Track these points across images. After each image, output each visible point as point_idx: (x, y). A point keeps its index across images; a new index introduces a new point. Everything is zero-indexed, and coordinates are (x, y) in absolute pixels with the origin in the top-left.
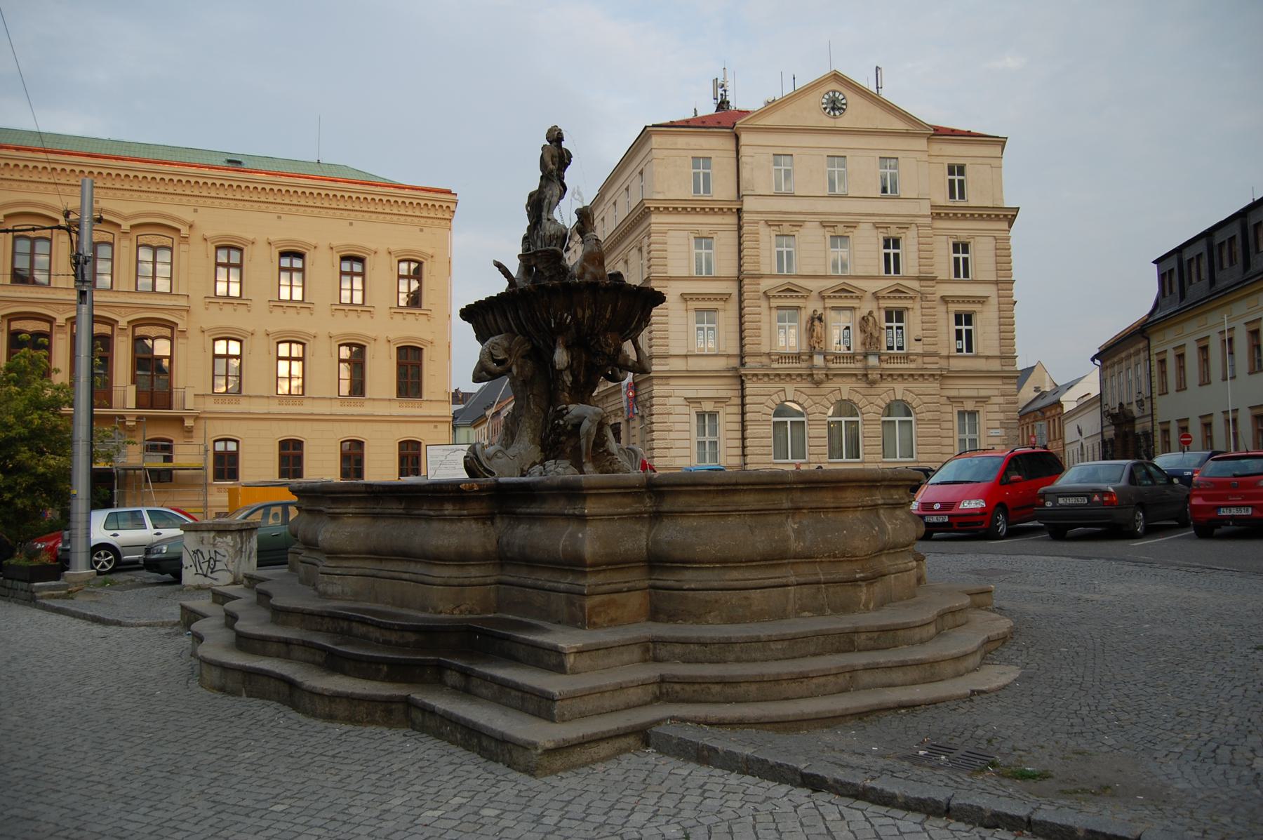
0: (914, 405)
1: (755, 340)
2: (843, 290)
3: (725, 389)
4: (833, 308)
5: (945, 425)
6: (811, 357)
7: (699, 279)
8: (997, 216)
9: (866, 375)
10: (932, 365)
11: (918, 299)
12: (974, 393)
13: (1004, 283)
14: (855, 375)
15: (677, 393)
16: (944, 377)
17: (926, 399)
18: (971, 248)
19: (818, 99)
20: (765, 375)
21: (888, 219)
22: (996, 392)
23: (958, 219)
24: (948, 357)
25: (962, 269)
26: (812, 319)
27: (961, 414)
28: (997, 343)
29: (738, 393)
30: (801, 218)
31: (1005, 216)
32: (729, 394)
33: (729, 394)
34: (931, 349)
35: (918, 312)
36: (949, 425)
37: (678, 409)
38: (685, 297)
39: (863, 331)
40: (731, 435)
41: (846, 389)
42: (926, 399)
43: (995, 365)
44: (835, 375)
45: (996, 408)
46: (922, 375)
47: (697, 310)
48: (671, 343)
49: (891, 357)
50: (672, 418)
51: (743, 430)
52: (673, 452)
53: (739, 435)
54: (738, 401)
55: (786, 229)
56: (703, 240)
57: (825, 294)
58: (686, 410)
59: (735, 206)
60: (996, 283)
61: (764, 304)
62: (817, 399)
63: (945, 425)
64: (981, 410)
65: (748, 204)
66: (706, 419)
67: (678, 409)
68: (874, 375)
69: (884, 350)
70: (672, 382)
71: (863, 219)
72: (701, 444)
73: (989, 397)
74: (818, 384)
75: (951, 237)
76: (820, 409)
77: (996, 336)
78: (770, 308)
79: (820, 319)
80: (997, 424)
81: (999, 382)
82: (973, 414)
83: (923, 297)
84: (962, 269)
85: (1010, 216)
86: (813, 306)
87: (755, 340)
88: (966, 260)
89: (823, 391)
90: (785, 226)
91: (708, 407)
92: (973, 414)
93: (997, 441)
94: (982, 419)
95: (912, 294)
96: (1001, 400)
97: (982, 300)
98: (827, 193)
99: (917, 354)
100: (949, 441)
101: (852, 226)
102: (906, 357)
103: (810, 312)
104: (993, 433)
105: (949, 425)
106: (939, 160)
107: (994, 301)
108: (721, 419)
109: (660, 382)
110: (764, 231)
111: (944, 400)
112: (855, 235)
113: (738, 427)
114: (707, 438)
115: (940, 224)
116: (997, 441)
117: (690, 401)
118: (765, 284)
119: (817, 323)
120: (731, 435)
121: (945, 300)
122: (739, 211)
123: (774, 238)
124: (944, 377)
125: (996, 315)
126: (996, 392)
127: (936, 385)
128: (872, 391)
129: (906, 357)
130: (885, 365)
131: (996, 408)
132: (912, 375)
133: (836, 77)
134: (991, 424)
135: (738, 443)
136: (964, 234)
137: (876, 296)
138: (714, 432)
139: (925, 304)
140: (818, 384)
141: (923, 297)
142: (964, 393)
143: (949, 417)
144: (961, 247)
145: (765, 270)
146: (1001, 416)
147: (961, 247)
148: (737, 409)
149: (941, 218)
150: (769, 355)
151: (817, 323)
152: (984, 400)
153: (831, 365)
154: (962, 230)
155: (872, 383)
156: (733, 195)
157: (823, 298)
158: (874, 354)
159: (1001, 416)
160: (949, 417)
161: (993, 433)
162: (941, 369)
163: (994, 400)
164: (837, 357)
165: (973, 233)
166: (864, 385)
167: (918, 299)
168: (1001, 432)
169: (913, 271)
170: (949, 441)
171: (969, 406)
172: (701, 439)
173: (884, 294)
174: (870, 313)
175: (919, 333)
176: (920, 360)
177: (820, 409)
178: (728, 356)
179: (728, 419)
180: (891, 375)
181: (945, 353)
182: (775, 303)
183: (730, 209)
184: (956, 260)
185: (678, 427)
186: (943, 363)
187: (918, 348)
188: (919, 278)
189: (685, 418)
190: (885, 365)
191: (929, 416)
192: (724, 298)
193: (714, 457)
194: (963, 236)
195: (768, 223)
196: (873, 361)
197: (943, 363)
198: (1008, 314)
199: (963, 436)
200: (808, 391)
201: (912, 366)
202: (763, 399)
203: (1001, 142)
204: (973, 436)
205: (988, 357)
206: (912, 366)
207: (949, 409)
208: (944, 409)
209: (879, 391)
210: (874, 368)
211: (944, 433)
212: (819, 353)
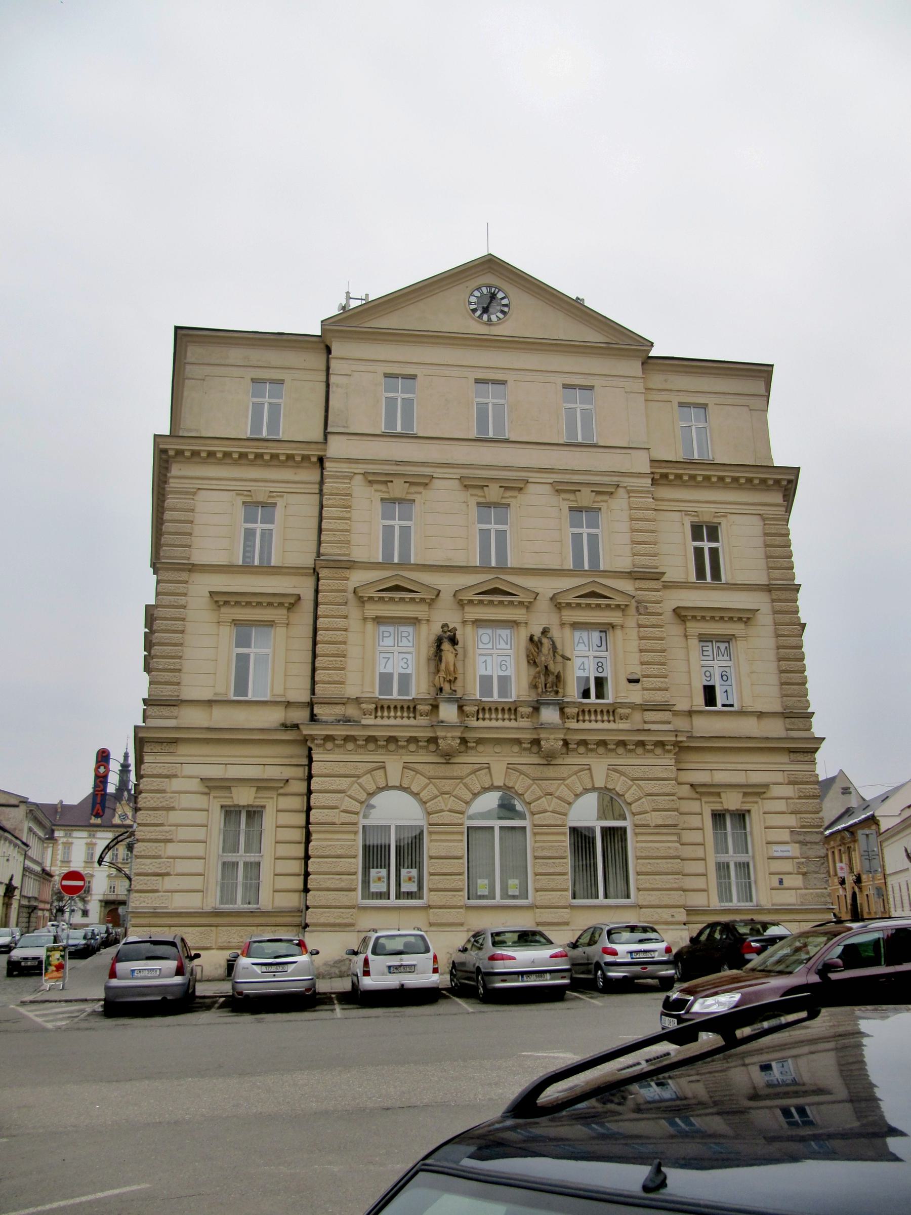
0: (629, 797)
1: (335, 675)
2: (397, 588)
3: (272, 763)
4: (478, 623)
5: (688, 837)
6: (435, 707)
7: (246, 568)
8: (721, 479)
9: (536, 742)
10: (660, 725)
11: (632, 610)
12: (739, 778)
13: (783, 590)
14: (518, 742)
15: (188, 770)
16: (682, 749)
17: (650, 787)
18: (722, 533)
19: (466, 296)
20: (347, 739)
21: (577, 478)
22: (779, 777)
23: (698, 486)
24: (690, 713)
25: (708, 567)
26: (439, 641)
27: (718, 817)
28: (774, 691)
29: (301, 772)
30: (427, 471)
31: (777, 482)
32: (288, 772)
33: (288, 772)
34: (659, 697)
35: (633, 633)
36: (696, 837)
37: (186, 801)
38: (220, 600)
39: (532, 662)
40: (283, 850)
41: (499, 765)
42: (650, 787)
43: (775, 728)
44: (480, 741)
45: (781, 806)
46: (642, 744)
47: (235, 623)
48: (186, 679)
49: (583, 712)
50: (174, 817)
51: (308, 840)
52: (169, 883)
53: (300, 851)
54: (302, 787)
55: (398, 489)
56: (259, 507)
57: (563, 600)
58: (200, 801)
59: (314, 452)
60: (768, 588)
61: (354, 612)
62: (447, 785)
63: (688, 837)
64: (754, 809)
65: (337, 447)
66: (243, 818)
67: (186, 801)
68: (552, 742)
69: (572, 692)
70: (183, 749)
71: (534, 477)
72: (229, 867)
73: (767, 786)
74: (448, 757)
75: (239, 493)
76: (452, 803)
77: (773, 679)
78: (365, 619)
79: (453, 641)
80: (785, 835)
81: (784, 758)
82: (741, 817)
83: (641, 608)
84: (708, 567)
85: (785, 483)
86: (445, 615)
87: (335, 675)
88: (714, 552)
89: (457, 771)
90: (400, 486)
91: (244, 797)
92: (741, 817)
93: (788, 866)
94: (755, 823)
95: (619, 600)
96: (788, 791)
97: (746, 617)
98: (474, 434)
99: (633, 706)
100: (698, 867)
101: (516, 486)
102: (611, 712)
103: (437, 629)
104: (777, 851)
105: (696, 837)
106: (664, 396)
107: (765, 619)
108: (268, 820)
109: (158, 748)
110: (359, 488)
111: (685, 790)
112: (517, 502)
113: (299, 835)
114: (242, 857)
115: (665, 492)
116: (788, 866)
117: (211, 785)
118: (357, 578)
119: (446, 646)
120: (283, 850)
121: (681, 615)
122: (321, 460)
123: (566, 511)
124: (682, 749)
125: (771, 643)
126: (779, 777)
127: (668, 760)
128: (550, 772)
129: (611, 712)
130: (573, 724)
131: (781, 806)
132: (623, 743)
133: (490, 264)
134: (774, 835)
135: (297, 867)
136: (712, 508)
137: (557, 603)
138: (743, 845)
139: (644, 620)
140: (448, 757)
141: (641, 608)
142: (721, 777)
143: (695, 821)
144: (705, 530)
145: (358, 554)
146: (792, 821)
147: (705, 530)
148: (298, 803)
149: (670, 484)
150: (358, 701)
151: (446, 646)
152: (758, 791)
153: (473, 723)
154: (707, 502)
155: (549, 759)
156: (318, 435)
157: (559, 607)
158: (548, 704)
159: (792, 821)
160: (695, 821)
161: (777, 851)
162: (676, 732)
163: (776, 791)
164: (483, 710)
165: (722, 508)
166: (535, 760)
167: (632, 610)
168: (793, 850)
169: (624, 563)
170: (698, 867)
171: (732, 801)
172: (231, 857)
173: (570, 598)
174: (545, 632)
175: (636, 670)
176: (637, 716)
177: (452, 803)
178: (288, 704)
179: (279, 821)
180: (584, 743)
181: (682, 705)
182: (373, 610)
183: (306, 458)
184: (699, 552)
185: (183, 833)
186: (681, 723)
187: (635, 695)
188: (633, 575)
189: (199, 817)
190: (573, 724)
191: (656, 818)
192: (292, 603)
193: (747, 893)
194: (707, 513)
195: (371, 479)
196: (550, 715)
197: (681, 723)
198: (792, 641)
199: (723, 858)
200: (430, 770)
201: (622, 725)
202: (343, 783)
203: (762, 373)
204: (742, 858)
205: (761, 715)
206: (622, 725)
207: (695, 806)
208: (686, 806)
209: (564, 771)
210: (553, 728)
211: (687, 852)
212: (449, 700)
